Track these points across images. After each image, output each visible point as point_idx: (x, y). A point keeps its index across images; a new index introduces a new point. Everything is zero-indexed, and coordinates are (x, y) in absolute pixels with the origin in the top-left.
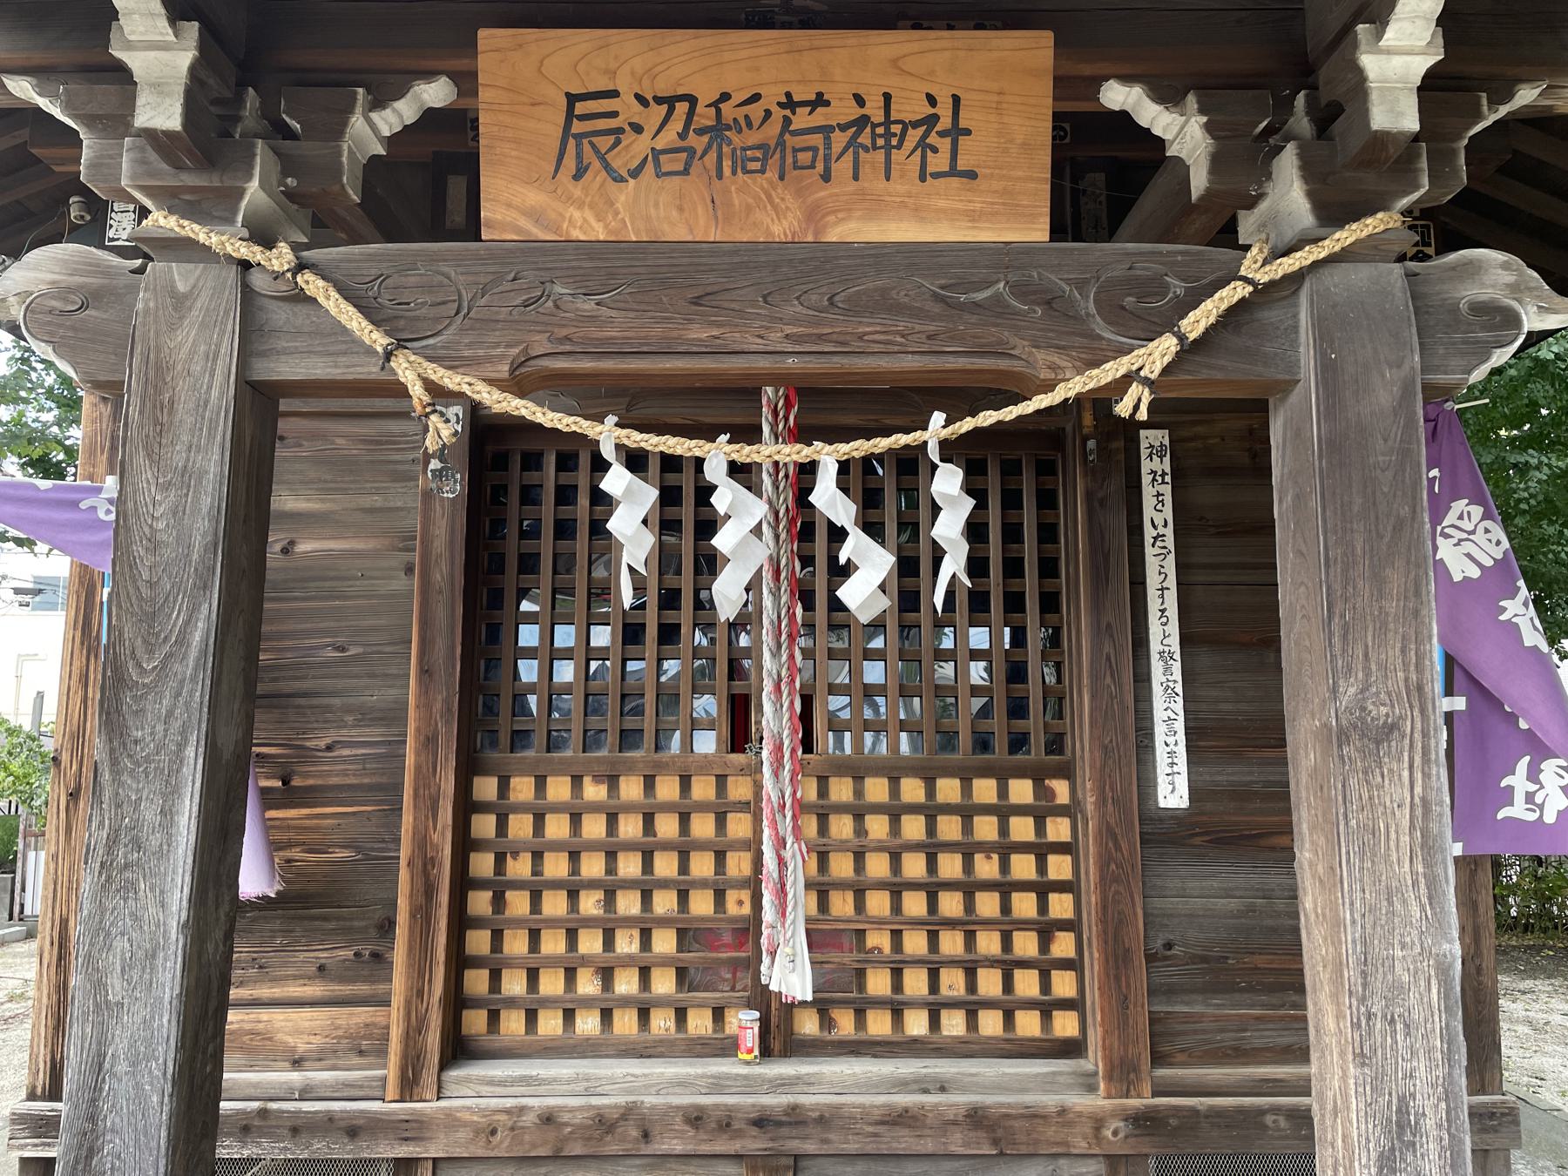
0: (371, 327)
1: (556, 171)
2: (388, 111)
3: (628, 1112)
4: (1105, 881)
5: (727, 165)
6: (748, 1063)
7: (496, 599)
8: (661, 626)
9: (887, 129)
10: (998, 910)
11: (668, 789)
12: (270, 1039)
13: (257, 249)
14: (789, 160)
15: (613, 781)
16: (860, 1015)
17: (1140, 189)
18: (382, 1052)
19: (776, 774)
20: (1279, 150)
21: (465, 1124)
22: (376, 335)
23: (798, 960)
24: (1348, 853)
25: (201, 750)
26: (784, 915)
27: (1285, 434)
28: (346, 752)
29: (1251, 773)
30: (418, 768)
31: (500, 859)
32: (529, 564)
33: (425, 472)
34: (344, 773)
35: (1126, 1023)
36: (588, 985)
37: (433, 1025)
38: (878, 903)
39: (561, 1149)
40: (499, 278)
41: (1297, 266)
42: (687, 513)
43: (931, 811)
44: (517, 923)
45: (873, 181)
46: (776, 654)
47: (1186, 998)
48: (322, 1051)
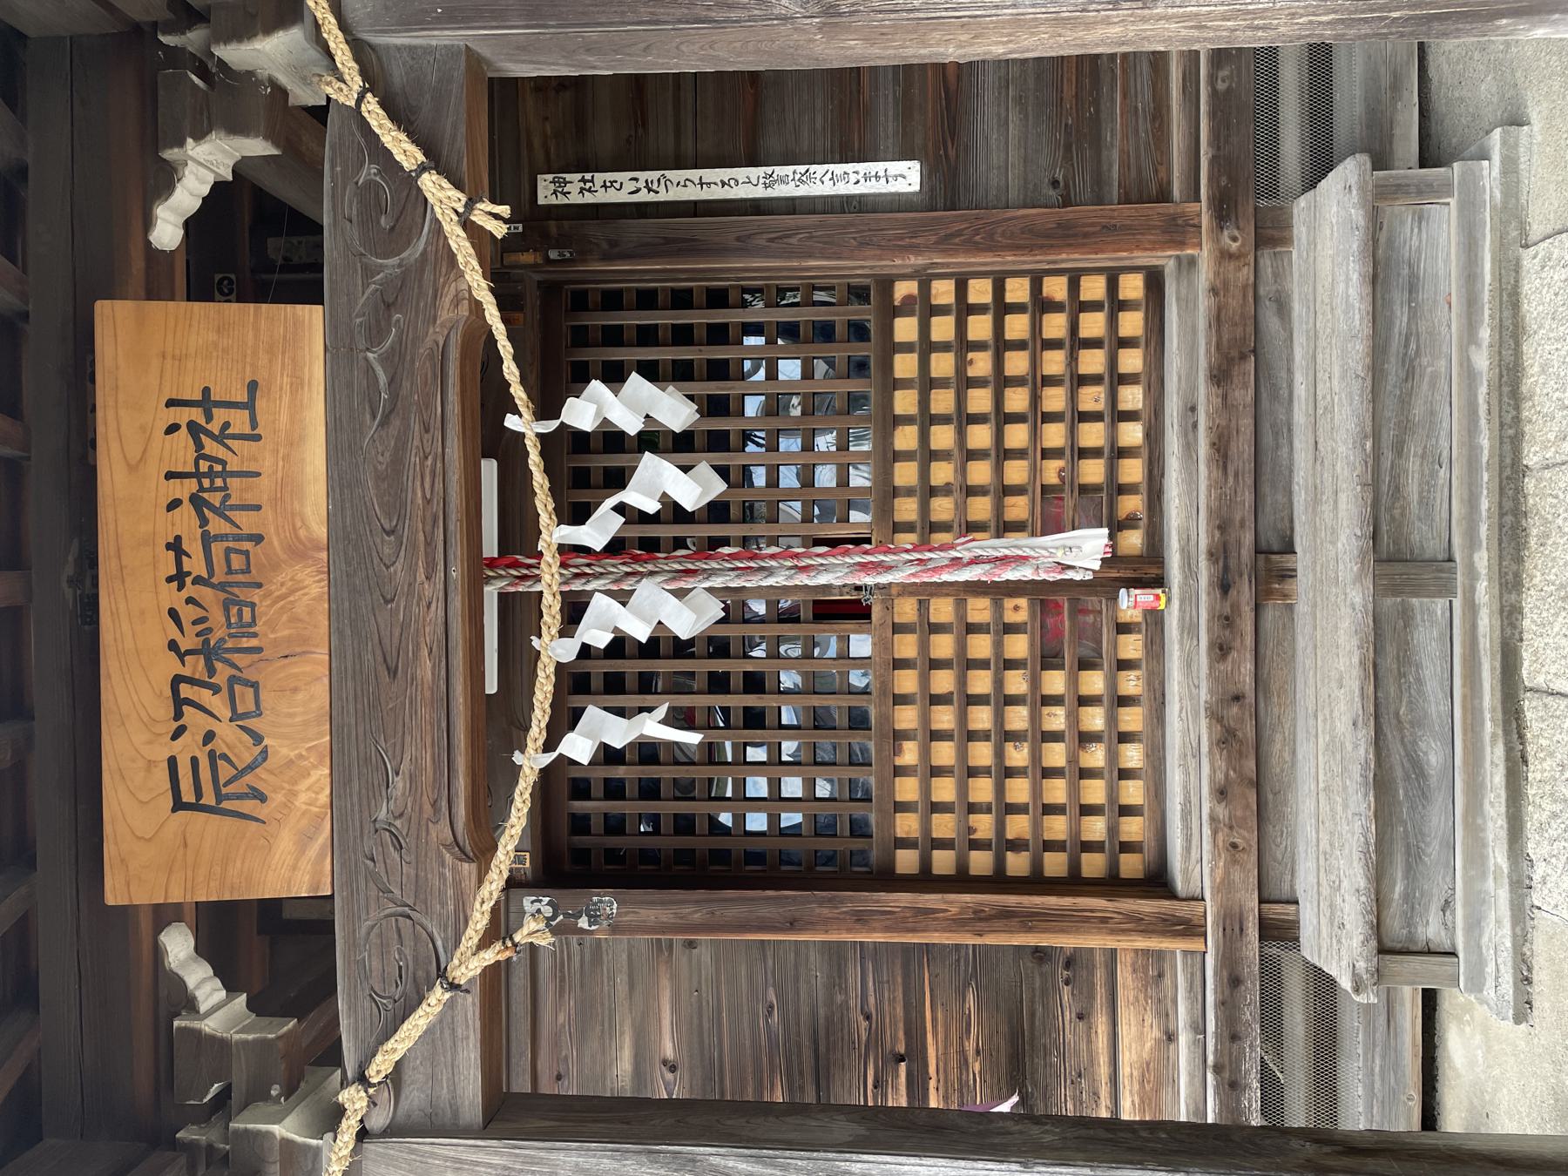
0: (424, 1006)
1: (257, 820)
2: (197, 994)
3: (1215, 716)
4: (992, 247)
5: (246, 643)
6: (1169, 600)
7: (720, 856)
8: (747, 691)
9: (205, 475)
10: (1022, 353)
11: (907, 682)
12: (1148, 1064)
13: (344, 1124)
14: (241, 578)
15: (899, 736)
16: (1123, 489)
17: (279, 205)
18: (1159, 955)
19: (889, 568)
20: (222, 64)
21: (1227, 873)
22: (432, 1000)
23: (1069, 543)
24: (946, 9)
25: (854, 1157)
26: (1026, 558)
27: (523, 62)
28: (872, 1000)
29: (886, 96)
30: (887, 929)
31: (976, 845)
32: (684, 825)
33: (592, 932)
34: (892, 1001)
35: (1129, 227)
36: (1096, 756)
37: (1135, 907)
38: (1016, 472)
39: (1250, 780)
40: (372, 876)
41: (345, 47)
42: (631, 667)
43: (927, 420)
44: (1037, 826)
45: (260, 492)
46: (770, 572)
47: (1105, 168)
48: (1158, 1014)
